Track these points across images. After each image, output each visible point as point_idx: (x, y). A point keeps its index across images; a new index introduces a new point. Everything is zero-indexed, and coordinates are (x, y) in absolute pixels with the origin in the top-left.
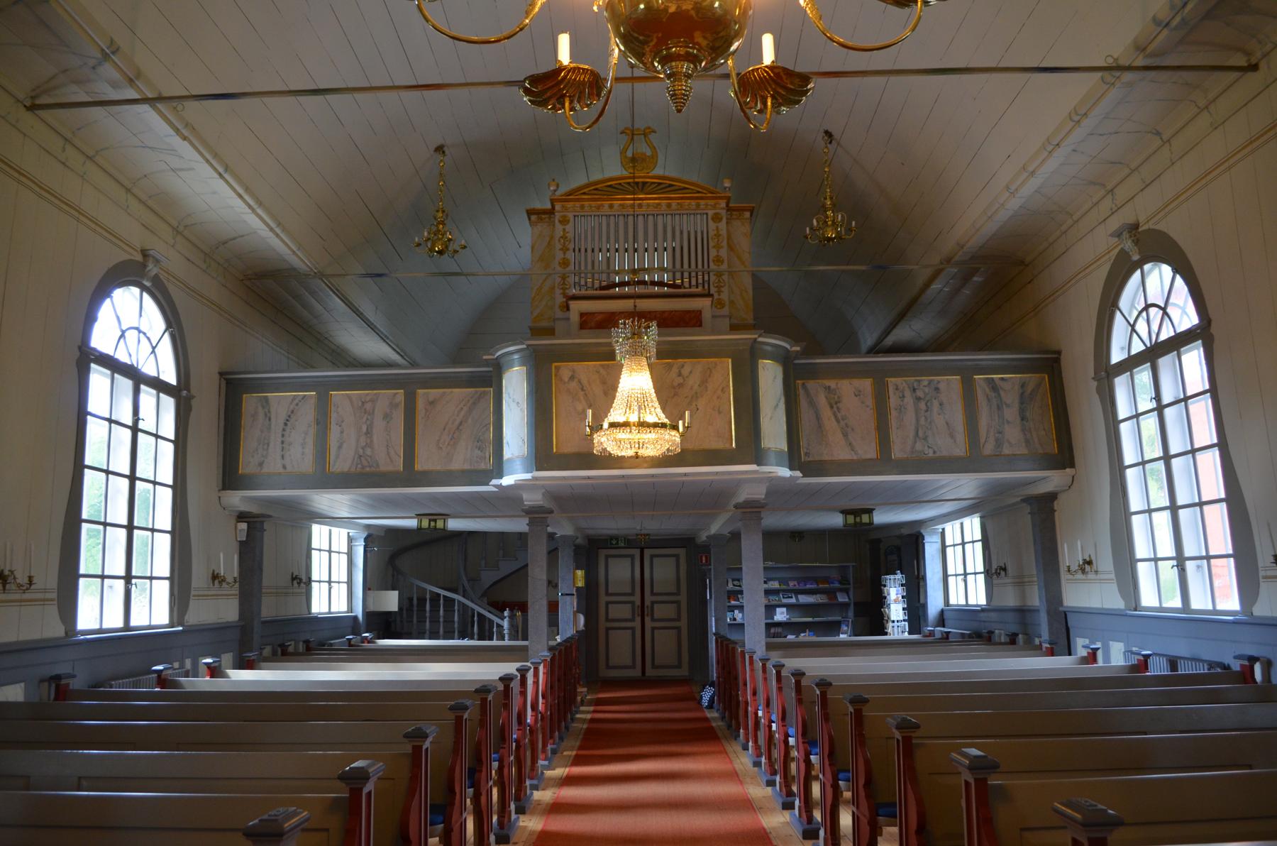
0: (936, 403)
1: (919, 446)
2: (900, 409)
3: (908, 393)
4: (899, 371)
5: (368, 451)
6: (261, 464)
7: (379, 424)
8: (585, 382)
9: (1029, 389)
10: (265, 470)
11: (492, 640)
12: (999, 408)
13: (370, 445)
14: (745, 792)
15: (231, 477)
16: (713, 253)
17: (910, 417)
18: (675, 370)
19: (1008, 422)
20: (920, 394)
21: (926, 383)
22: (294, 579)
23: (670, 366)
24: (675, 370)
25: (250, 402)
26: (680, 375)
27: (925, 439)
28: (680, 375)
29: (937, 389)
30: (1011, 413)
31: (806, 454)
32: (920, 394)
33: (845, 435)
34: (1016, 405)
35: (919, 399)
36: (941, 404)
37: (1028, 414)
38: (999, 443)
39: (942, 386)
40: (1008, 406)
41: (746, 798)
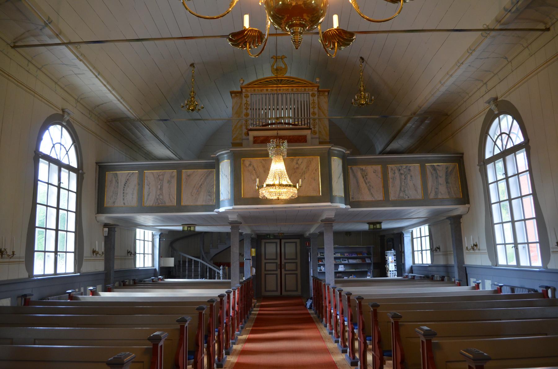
0: (409, 176)
1: (401, 195)
2: (393, 178)
3: (397, 171)
4: (393, 162)
5: (161, 197)
6: (114, 203)
7: (166, 185)
8: (255, 167)
9: (450, 170)
10: (116, 205)
11: (215, 279)
12: (437, 178)
13: (162, 194)
14: (326, 345)
15: (101, 208)
16: (312, 110)
17: (398, 182)
18: (295, 161)
19: (441, 184)
20: (402, 172)
21: (404, 167)
22: (128, 252)
23: (293, 160)
24: (295, 161)
25: (109, 175)
26: (297, 163)
27: (404, 191)
28: (297, 163)
29: (409, 170)
30: (442, 180)
31: (352, 198)
32: (402, 172)
33: (369, 190)
34: (444, 177)
35: (401, 174)
36: (411, 176)
37: (449, 181)
38: (436, 193)
39: (412, 168)
40: (440, 177)
41: (326, 348)
